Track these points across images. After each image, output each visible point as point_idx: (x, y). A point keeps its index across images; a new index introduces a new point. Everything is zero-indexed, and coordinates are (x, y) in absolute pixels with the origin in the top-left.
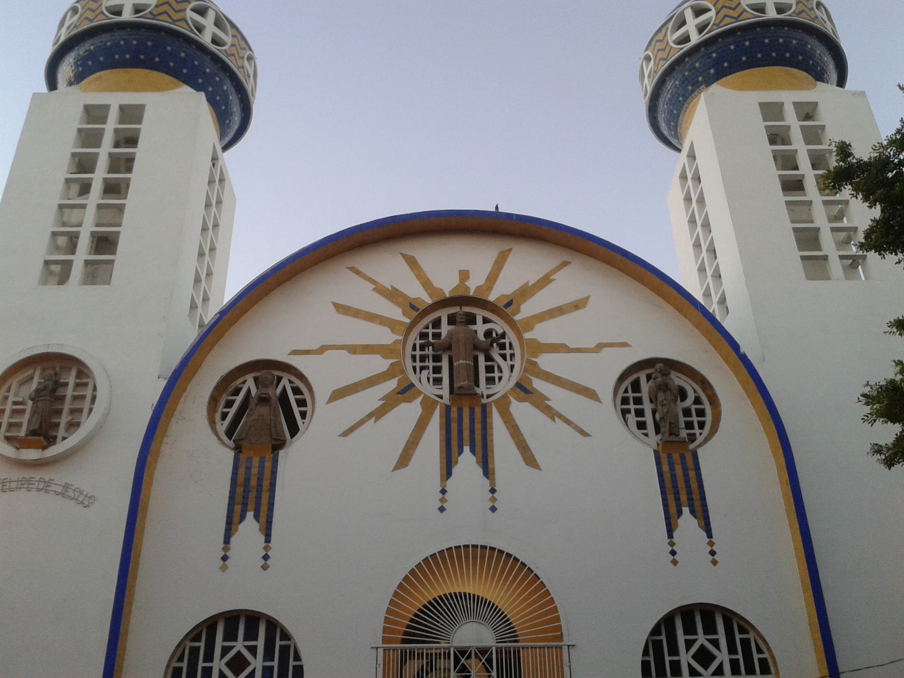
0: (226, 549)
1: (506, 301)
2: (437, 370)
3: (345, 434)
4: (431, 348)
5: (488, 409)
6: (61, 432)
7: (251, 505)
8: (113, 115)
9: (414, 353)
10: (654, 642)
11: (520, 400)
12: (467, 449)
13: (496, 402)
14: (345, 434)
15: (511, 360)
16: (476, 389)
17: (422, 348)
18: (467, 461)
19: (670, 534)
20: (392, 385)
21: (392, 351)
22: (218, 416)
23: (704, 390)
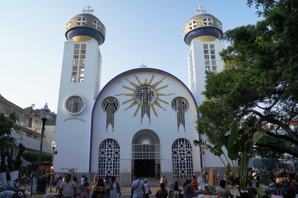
2: (141, 98)
3: (125, 110)
12: (146, 113)
14: (125, 110)
18: (146, 115)
19: (178, 127)
20: (133, 101)
22: (103, 106)
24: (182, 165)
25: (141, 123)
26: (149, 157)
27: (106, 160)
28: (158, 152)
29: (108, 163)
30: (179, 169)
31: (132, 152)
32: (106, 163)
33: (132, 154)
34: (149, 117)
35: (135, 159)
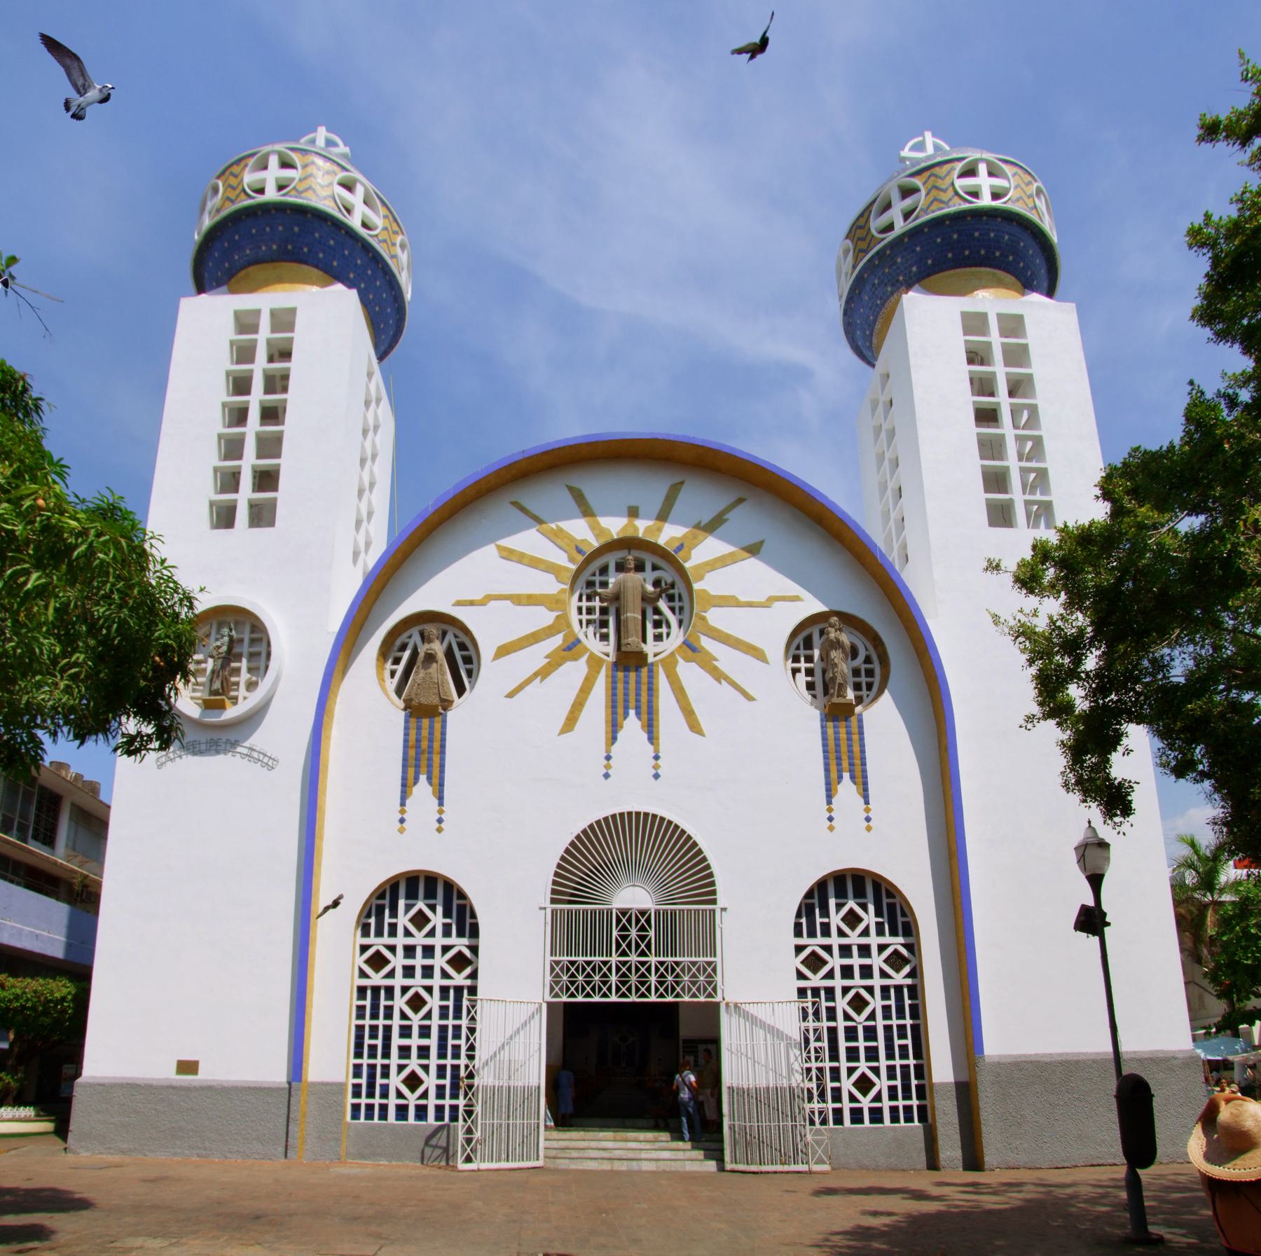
0: (403, 812)
1: (676, 544)
2: (604, 624)
3: (511, 695)
4: (597, 598)
5: (655, 668)
6: (242, 691)
7: (424, 769)
8: (265, 323)
9: (580, 604)
10: (807, 905)
11: (687, 660)
12: (632, 712)
13: (662, 661)
14: (511, 695)
15: (680, 614)
16: (643, 645)
17: (589, 599)
18: (632, 726)
19: (829, 802)
20: (557, 641)
21: (557, 601)
22: (387, 674)
23: (875, 647)
24: (856, 1039)
25: (607, 776)
26: (649, 989)
27: (400, 1003)
28: (690, 955)
29: (410, 1027)
30: (844, 1064)
31: (549, 958)
32: (396, 1022)
33: (552, 969)
34: (652, 738)
35: (565, 1003)
